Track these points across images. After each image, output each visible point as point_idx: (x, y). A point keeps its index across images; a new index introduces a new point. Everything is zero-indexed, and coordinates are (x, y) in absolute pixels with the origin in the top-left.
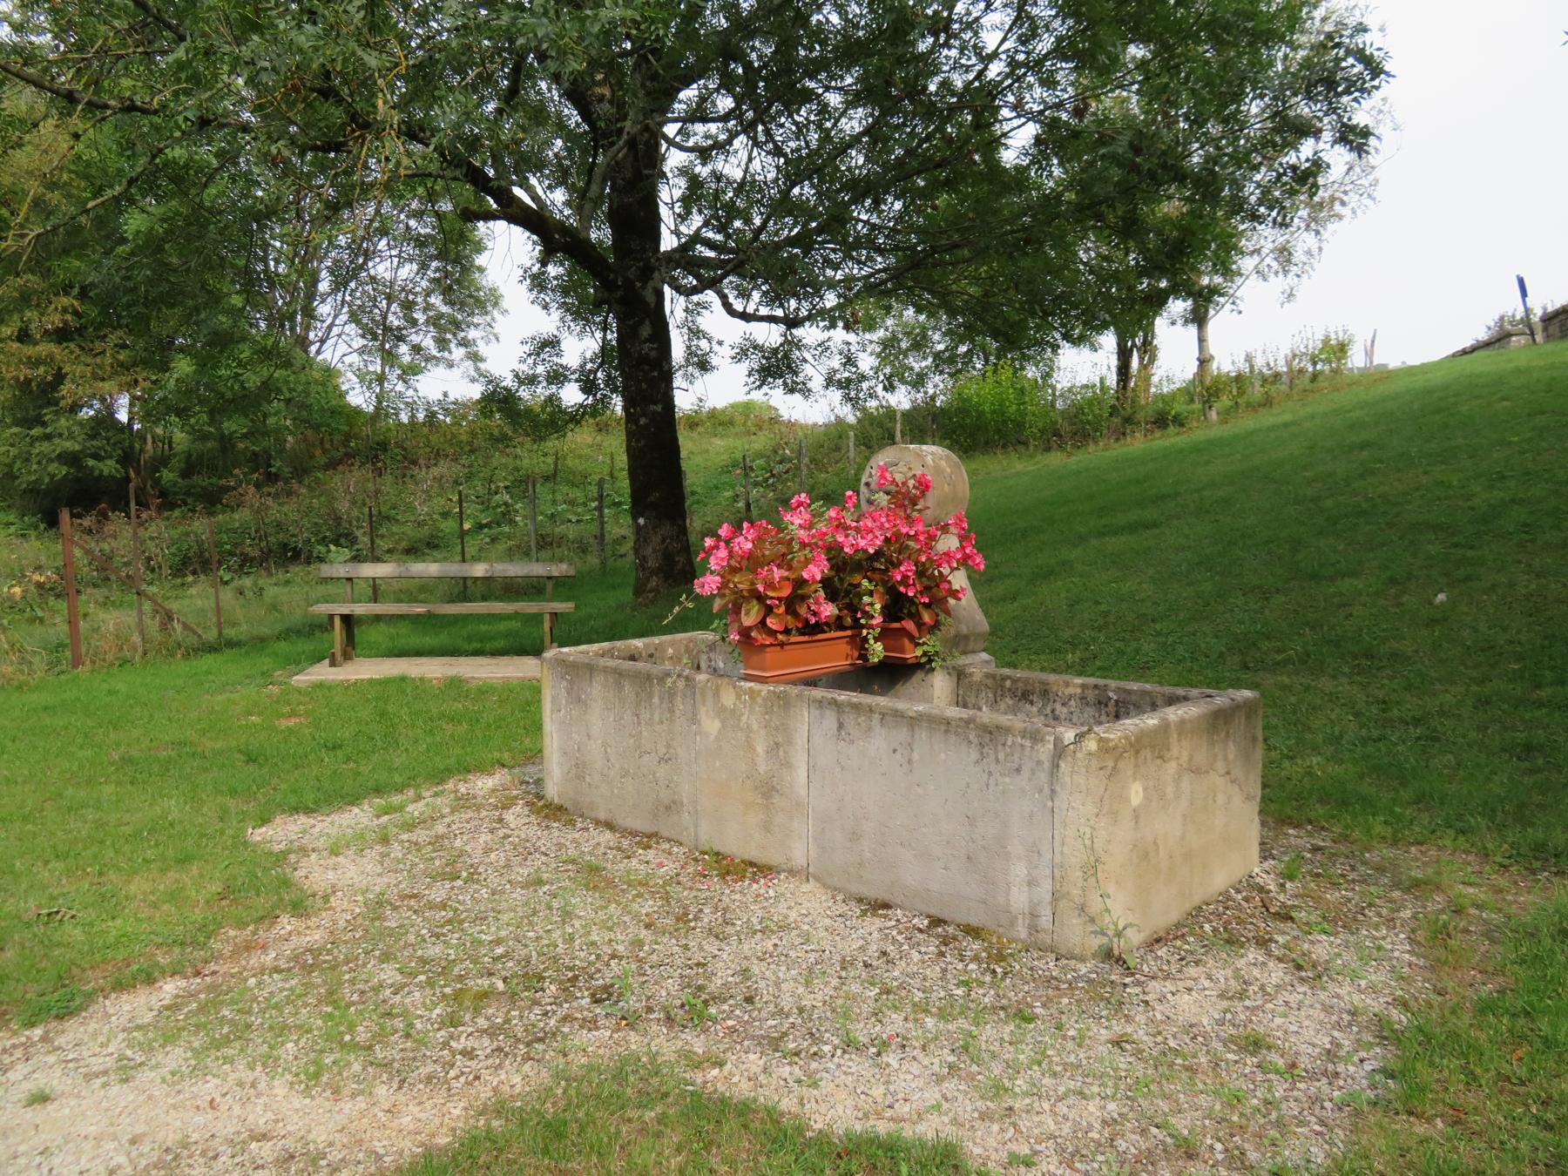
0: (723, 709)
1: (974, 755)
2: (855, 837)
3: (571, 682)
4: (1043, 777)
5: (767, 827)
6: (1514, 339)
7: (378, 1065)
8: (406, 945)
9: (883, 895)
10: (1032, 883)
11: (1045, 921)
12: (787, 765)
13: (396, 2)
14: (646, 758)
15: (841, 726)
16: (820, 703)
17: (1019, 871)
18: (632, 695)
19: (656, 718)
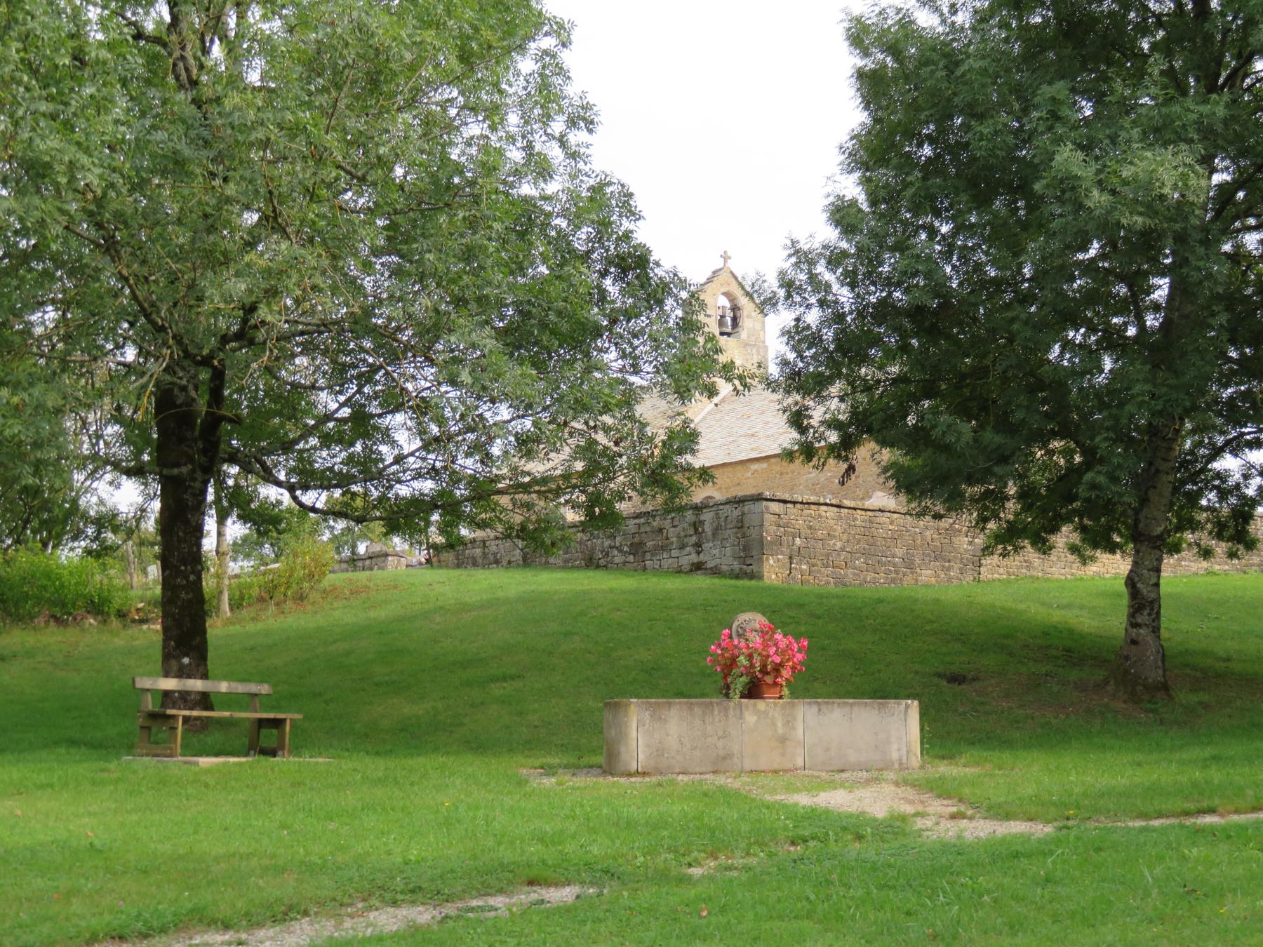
0: (759, 711)
1: (876, 712)
2: (828, 749)
3: (654, 711)
4: (902, 716)
5: (783, 755)
6: (390, 558)
7: (153, 323)
8: (475, 929)
9: (841, 767)
10: (899, 750)
11: (904, 760)
12: (794, 728)
13: (1043, 4)
14: (709, 739)
15: (820, 710)
16: (810, 703)
17: (895, 746)
18: (700, 712)
19: (717, 720)
